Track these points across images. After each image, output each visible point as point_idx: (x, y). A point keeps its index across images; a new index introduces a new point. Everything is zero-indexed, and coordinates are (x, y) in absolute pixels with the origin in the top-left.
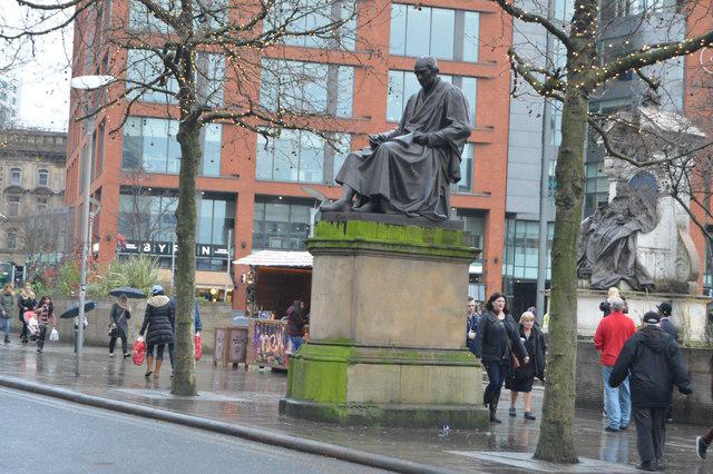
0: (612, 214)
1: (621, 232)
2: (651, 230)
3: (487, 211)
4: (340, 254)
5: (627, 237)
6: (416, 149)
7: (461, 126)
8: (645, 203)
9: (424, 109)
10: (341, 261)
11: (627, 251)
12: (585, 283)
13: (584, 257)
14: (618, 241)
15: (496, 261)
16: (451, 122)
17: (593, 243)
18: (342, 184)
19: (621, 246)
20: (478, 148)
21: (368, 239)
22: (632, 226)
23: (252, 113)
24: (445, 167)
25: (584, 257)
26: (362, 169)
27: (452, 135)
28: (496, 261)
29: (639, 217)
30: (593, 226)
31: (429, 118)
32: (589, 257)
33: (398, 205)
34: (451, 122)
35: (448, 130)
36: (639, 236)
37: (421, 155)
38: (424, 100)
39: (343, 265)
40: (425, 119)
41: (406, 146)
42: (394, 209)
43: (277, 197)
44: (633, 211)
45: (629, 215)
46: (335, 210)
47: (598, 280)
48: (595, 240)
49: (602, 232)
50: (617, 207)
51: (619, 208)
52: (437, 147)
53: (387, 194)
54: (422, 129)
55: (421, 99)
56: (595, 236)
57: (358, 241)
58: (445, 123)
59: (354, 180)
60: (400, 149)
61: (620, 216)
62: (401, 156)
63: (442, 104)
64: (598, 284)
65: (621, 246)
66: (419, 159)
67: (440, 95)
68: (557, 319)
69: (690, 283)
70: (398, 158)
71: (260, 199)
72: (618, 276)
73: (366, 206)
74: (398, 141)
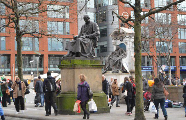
0: (116, 54)
1: (118, 58)
2: (125, 57)
3: (176, 56)
4: (69, 69)
5: (120, 60)
6: (86, 39)
7: (97, 33)
8: (123, 51)
9: (87, 29)
10: (70, 70)
11: (120, 63)
12: (111, 72)
13: (109, 65)
14: (118, 61)
15: (46, 68)
16: (94, 32)
17: (111, 61)
18: (67, 50)
19: (119, 62)
20: (7, 38)
21: (77, 64)
22: (121, 57)
23: (35, 32)
24: (94, 44)
25: (109, 65)
26: (72, 45)
27: (95, 35)
28: (46, 68)
29: (122, 54)
30: (111, 57)
31: (89, 31)
32: (111, 65)
33: (83, 55)
34: (94, 32)
35: (94, 34)
36: (123, 59)
37: (88, 41)
38: (86, 26)
39: (71, 72)
40: (87, 31)
41: (84, 38)
42: (82, 56)
43: (52, 55)
44: (120, 53)
45: (120, 54)
46: (66, 57)
47: (114, 71)
48: (112, 61)
49: (113, 58)
50: (116, 52)
51: (117, 52)
52: (91, 38)
53: (80, 51)
54: (87, 34)
55: (85, 26)
56: (112, 60)
57: (75, 65)
58: (93, 32)
59: (71, 48)
60: (83, 40)
61: (118, 54)
62: (84, 41)
63: (92, 27)
64: (114, 72)
65: (119, 62)
66: (88, 42)
67: (91, 25)
68: (138, 82)
69: (128, 71)
70: (83, 42)
71: (49, 56)
72: (119, 69)
73: (74, 56)
74: (82, 37)
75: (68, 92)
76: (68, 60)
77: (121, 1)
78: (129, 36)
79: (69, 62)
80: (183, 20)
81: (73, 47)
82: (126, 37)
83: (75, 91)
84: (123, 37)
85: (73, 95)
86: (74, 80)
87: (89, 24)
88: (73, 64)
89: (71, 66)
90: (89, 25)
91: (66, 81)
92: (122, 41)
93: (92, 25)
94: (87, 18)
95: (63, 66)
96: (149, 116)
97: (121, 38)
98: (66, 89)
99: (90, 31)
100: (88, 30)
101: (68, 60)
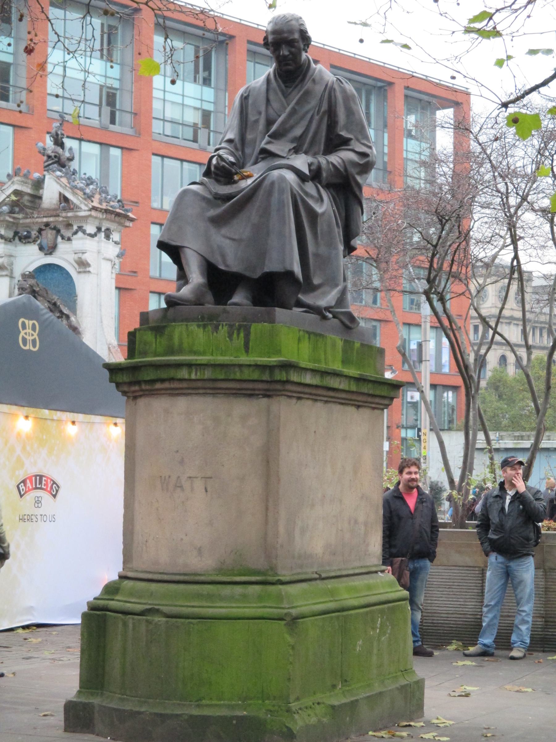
27: (355, 164)
57: (287, 366)
63: (325, 107)
75: (220, 571)
76: (223, 330)
77: (38, 2)
78: (99, 229)
79: (239, 341)
80: (515, 155)
81: (224, 231)
82: (80, 229)
83: (273, 569)
84: (58, 231)
85: (260, 598)
86: (267, 484)
87: (308, 85)
88: (274, 359)
89: (256, 375)
90: (307, 93)
91: (199, 485)
92: (50, 250)
93: (330, 91)
94: (296, 36)
95: (184, 373)
96: (86, 738)
97: (49, 234)
98: (200, 551)
99: (316, 133)
100: (304, 123)
101: (223, 330)
